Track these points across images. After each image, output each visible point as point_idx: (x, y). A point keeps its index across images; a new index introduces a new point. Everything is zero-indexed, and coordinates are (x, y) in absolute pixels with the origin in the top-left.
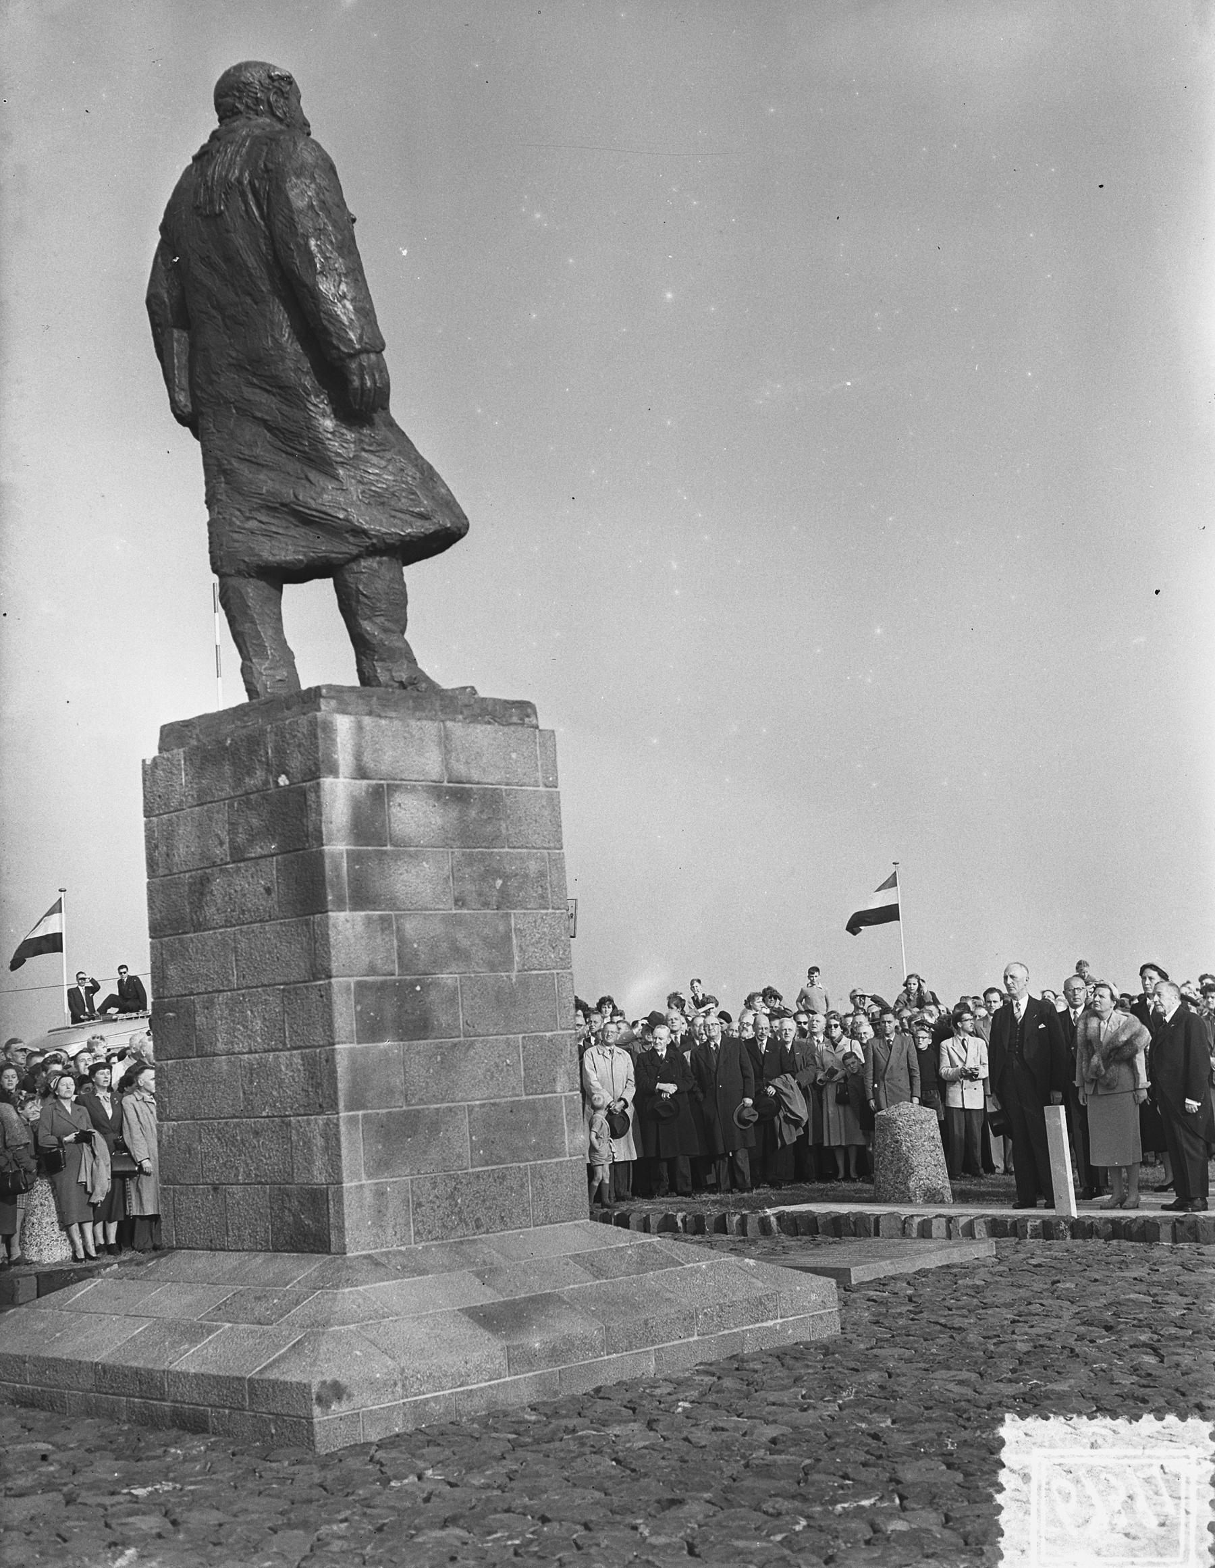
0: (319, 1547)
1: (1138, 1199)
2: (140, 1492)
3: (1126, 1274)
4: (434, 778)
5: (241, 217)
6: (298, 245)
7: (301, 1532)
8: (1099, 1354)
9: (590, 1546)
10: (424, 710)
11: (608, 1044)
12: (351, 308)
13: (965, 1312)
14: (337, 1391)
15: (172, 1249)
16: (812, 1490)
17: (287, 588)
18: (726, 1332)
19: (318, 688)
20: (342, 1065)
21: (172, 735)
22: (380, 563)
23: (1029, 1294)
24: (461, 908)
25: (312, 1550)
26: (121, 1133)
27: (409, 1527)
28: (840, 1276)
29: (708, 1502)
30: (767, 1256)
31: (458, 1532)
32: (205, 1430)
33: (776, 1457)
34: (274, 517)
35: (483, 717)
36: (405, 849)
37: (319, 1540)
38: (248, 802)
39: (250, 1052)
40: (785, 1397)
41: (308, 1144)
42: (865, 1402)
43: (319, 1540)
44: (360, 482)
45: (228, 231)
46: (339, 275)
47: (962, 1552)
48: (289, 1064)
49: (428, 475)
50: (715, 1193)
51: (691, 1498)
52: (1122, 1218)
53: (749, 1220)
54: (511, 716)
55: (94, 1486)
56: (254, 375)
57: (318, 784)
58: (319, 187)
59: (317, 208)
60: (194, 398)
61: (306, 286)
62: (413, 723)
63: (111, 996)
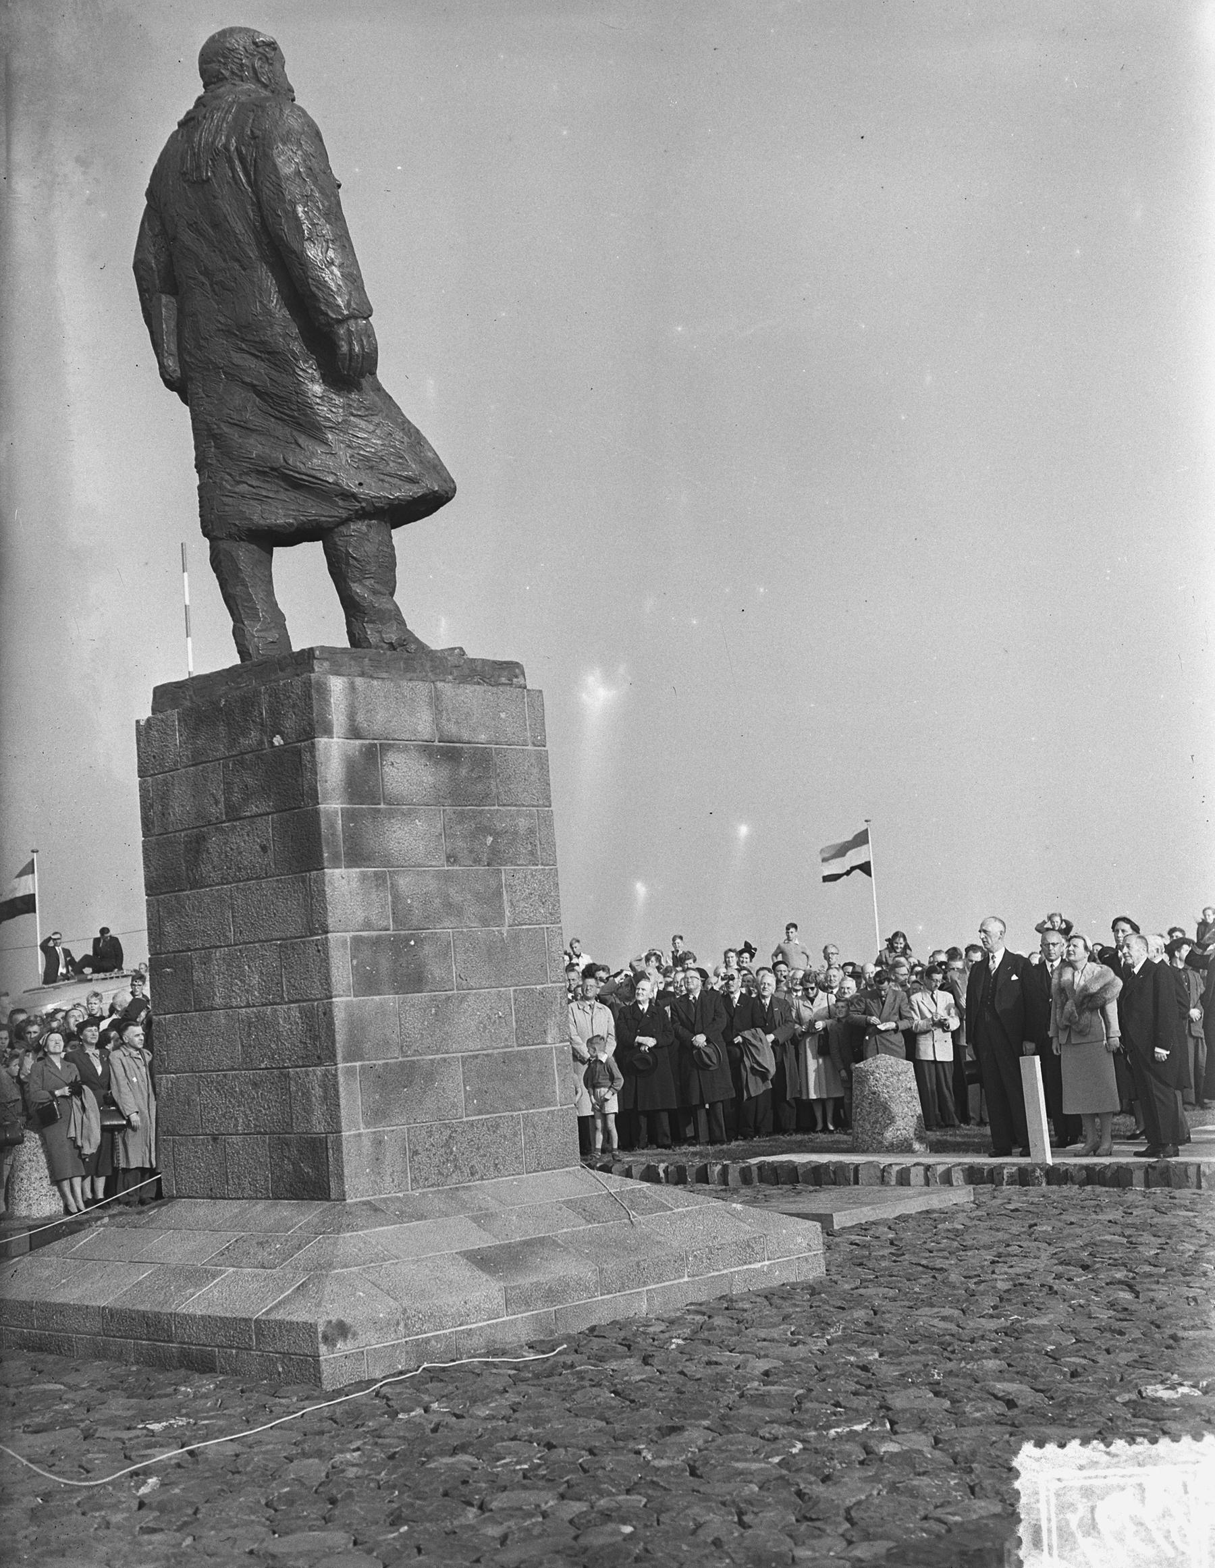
0: (335, 1474)
1: (1111, 1147)
2: (156, 1427)
3: (1100, 1217)
4: (426, 738)
5: (228, 183)
6: (286, 212)
7: (317, 1460)
8: (1077, 1291)
9: (597, 1469)
10: (414, 671)
11: (588, 999)
12: (338, 274)
13: (946, 1254)
14: (342, 1330)
15: (172, 1198)
16: (807, 1417)
17: (278, 551)
18: (717, 1273)
19: (311, 649)
20: (339, 1016)
21: (165, 695)
22: (369, 526)
23: (1007, 1236)
24: (453, 864)
25: (327, 1477)
26: (109, 1088)
27: (420, 1456)
28: (825, 1220)
29: (708, 1428)
30: (752, 1202)
31: (467, 1458)
32: (213, 1370)
33: (769, 1387)
34: (264, 481)
35: (473, 677)
36: (398, 807)
37: (333, 1467)
38: (242, 763)
39: (248, 1006)
40: (775, 1333)
41: (307, 1094)
42: (852, 1338)
43: (333, 1467)
44: (349, 446)
45: (215, 197)
46: (327, 242)
47: (950, 1469)
48: (288, 1017)
49: (416, 439)
50: (694, 1145)
51: (690, 1425)
52: (1095, 1164)
53: (730, 1171)
54: (499, 676)
55: (111, 1422)
56: (243, 340)
57: (313, 744)
58: (306, 154)
59: (304, 175)
60: (182, 363)
61: (294, 252)
62: (404, 683)
63: (86, 956)
